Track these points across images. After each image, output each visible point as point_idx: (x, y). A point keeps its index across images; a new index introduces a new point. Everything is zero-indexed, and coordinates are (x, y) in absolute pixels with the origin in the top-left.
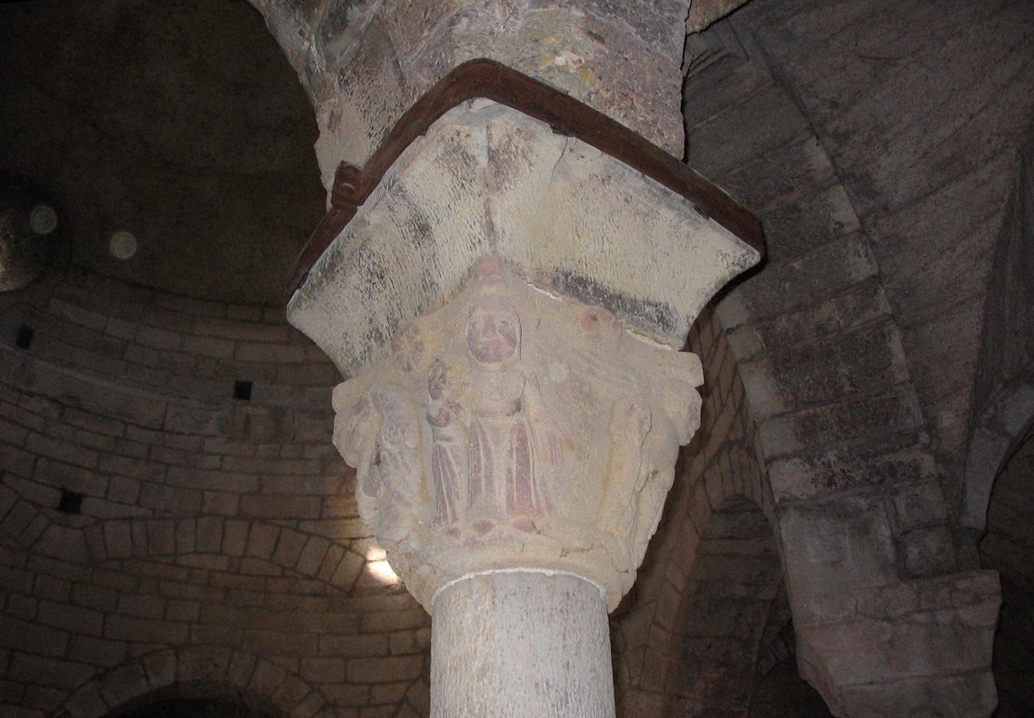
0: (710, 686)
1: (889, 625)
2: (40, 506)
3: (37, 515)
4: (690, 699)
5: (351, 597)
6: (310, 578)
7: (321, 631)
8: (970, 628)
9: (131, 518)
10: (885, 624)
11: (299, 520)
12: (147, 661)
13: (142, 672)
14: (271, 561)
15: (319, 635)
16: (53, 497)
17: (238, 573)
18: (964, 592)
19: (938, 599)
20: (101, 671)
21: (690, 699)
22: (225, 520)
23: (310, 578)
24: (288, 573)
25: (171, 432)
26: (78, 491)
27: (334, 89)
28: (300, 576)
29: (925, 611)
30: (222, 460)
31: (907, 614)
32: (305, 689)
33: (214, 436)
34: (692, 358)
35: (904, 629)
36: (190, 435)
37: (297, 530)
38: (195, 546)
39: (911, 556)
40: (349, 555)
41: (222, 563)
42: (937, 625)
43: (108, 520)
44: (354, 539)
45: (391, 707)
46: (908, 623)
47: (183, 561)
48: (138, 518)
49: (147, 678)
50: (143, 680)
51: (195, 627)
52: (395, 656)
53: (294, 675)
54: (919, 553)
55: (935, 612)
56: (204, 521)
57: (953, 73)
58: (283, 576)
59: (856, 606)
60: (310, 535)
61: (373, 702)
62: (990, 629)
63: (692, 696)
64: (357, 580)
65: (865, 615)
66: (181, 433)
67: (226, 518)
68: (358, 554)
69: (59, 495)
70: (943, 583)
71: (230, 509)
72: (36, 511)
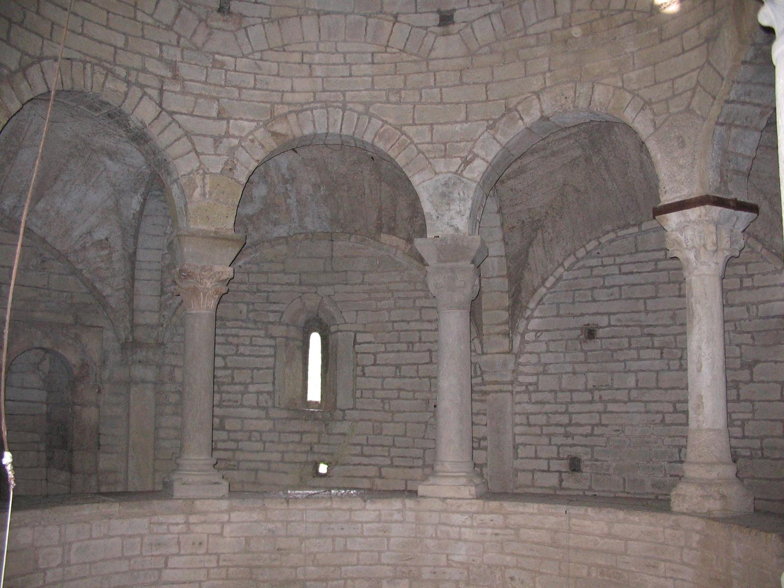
2: (427, 28)
3: (426, 35)
5: (652, 15)
6: (621, 11)
7: (634, 50)
9: (489, 14)
12: (520, 108)
13: (518, 116)
14: (591, 9)
15: (633, 53)
16: (434, 18)
20: (491, 122)
23: (621, 11)
24: (605, 13)
26: (449, 8)
28: (613, 13)
32: (628, 96)
34: (498, 216)
38: (537, 17)
43: (474, 21)
45: (689, 92)
47: (531, 31)
48: (494, 12)
49: (522, 119)
50: (520, 121)
51: (548, 75)
52: (688, 51)
57: (380, 177)
61: (676, 93)
69: (438, 16)
72: (425, 32)
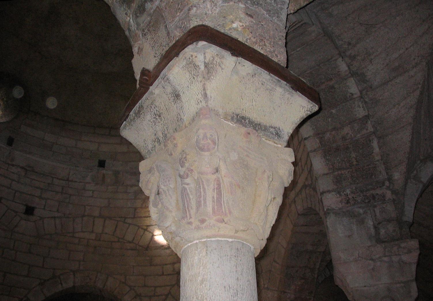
0: (298, 288)
1: (372, 262)
2: (17, 212)
3: (15, 216)
4: (289, 293)
5: (147, 250)
6: (130, 242)
7: (134, 264)
8: (406, 263)
9: (55, 217)
10: (370, 261)
11: (125, 218)
12: (62, 277)
13: (60, 282)
14: (113, 235)
15: (134, 266)
16: (22, 208)
17: (100, 240)
18: (404, 248)
19: (393, 251)
20: (42, 281)
21: (289, 293)
22: (94, 218)
23: (130, 242)
24: (121, 240)
25: (72, 181)
26: (33, 206)
27: (140, 37)
28: (126, 242)
29: (387, 256)
30: (93, 193)
31: (380, 258)
32: (128, 289)
33: (90, 183)
34: (290, 150)
35: (378, 263)
36: (80, 182)
37: (124, 222)
38: (82, 229)
39: (381, 233)
40: (146, 233)
41: (93, 236)
42: (393, 262)
43: (45, 218)
44: (148, 226)
45: (164, 296)
46: (380, 261)
47: (77, 235)
48: (58, 217)
49: (62, 284)
50: (60, 285)
51: (82, 263)
52: (165, 275)
53: (123, 283)
54: (385, 232)
55: (392, 257)
56: (85, 218)
57: (399, 31)
58: (118, 241)
59: (358, 254)
60: (130, 224)
61: (156, 294)
62: (415, 264)
63: (290, 292)
64: (149, 243)
65: (362, 258)
66: (76, 182)
67: (95, 217)
68: (150, 232)
69: (25, 208)
70: (395, 244)
71: (96, 213)
72: (15, 214)
